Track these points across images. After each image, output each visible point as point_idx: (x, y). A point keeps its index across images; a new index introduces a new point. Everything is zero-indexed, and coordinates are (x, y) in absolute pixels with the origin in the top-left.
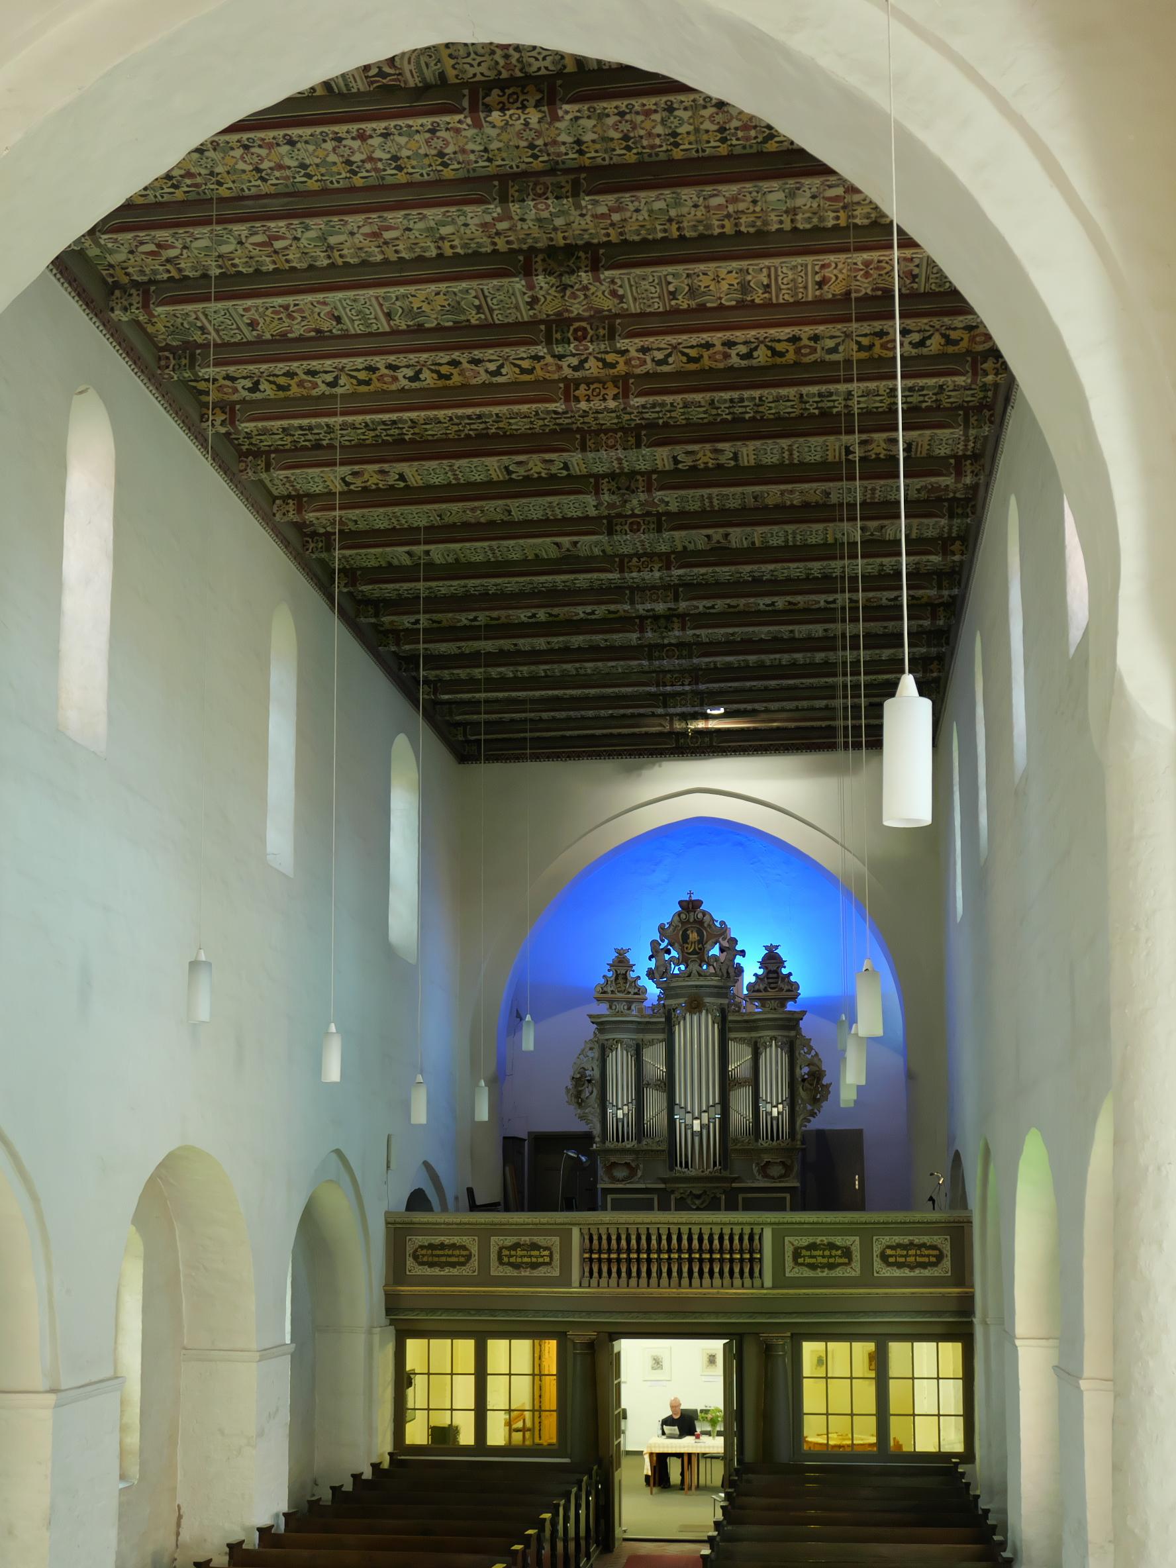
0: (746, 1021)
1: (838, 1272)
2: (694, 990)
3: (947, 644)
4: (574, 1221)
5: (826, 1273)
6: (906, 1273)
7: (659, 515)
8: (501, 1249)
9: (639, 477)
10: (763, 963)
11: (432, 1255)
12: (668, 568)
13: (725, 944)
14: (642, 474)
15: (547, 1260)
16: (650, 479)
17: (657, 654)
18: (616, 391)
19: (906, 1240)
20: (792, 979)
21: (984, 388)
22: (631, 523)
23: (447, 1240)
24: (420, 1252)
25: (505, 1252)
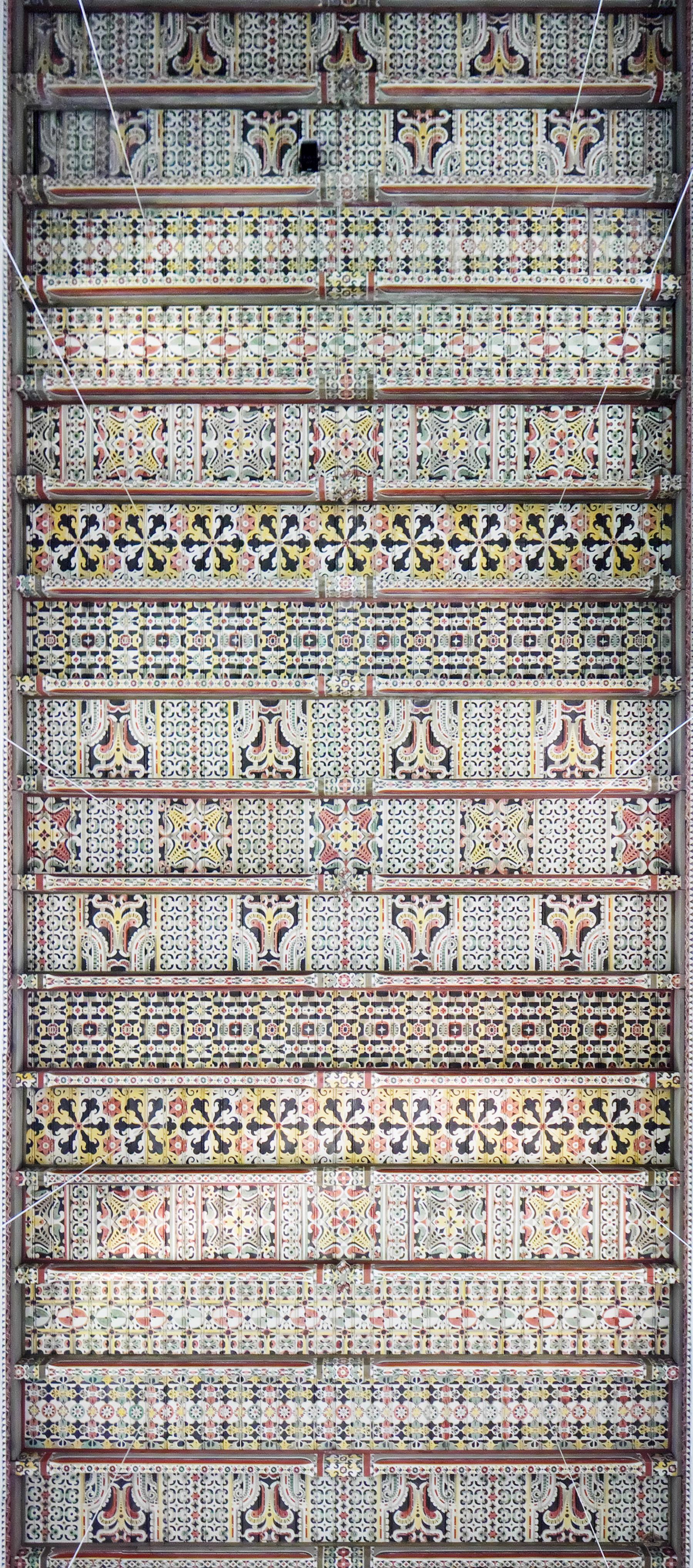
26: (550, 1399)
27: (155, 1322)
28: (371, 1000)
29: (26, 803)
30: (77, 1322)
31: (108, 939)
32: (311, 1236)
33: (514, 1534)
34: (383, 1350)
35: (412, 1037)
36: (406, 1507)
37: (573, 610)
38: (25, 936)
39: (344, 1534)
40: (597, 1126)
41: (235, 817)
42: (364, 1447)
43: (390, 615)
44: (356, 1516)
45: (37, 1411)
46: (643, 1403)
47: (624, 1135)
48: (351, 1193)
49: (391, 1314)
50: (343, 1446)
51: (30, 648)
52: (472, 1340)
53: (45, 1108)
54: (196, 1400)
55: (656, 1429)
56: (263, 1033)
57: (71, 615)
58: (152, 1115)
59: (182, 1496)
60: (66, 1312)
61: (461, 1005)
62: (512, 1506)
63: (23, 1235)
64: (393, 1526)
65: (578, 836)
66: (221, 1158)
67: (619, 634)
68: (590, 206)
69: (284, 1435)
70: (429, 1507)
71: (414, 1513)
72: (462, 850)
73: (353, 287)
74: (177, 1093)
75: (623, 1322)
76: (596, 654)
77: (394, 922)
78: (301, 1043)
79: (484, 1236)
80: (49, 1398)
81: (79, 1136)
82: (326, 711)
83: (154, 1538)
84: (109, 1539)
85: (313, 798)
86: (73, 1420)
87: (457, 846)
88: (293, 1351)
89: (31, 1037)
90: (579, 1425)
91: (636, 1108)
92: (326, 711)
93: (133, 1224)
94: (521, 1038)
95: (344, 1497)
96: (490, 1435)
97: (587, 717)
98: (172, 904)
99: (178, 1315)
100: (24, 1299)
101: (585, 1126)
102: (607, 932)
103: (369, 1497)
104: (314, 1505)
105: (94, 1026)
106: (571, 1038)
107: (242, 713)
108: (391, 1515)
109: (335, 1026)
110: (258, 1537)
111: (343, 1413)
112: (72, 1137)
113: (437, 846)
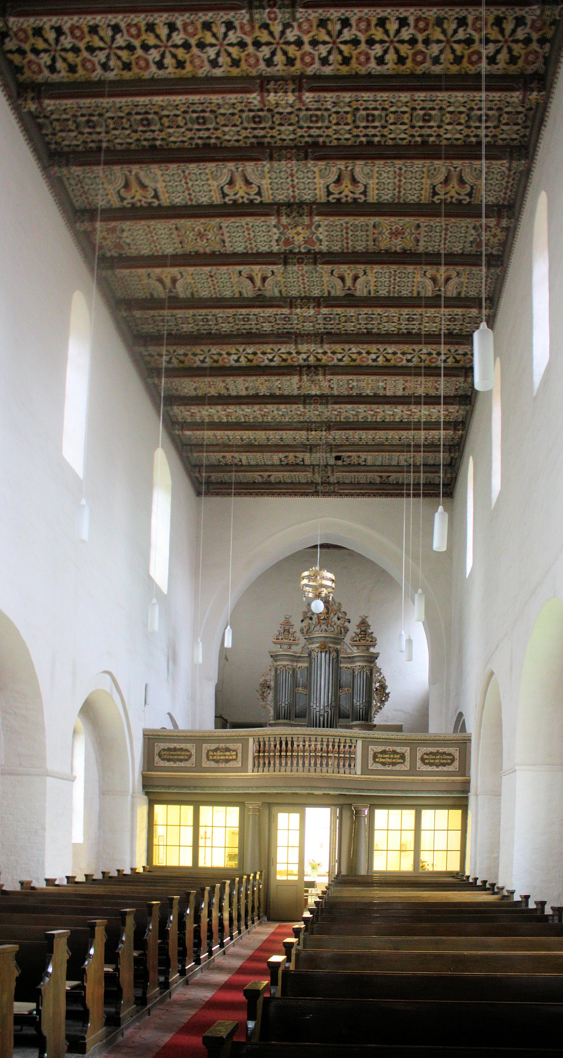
0: (349, 658)
1: (397, 768)
2: (323, 640)
3: (470, 404)
4: (251, 734)
5: (391, 768)
6: (434, 768)
7: (316, 254)
8: (208, 751)
9: (304, 206)
10: (359, 626)
11: (170, 755)
12: (319, 307)
13: (340, 615)
14: (307, 204)
15: (234, 757)
16: (311, 208)
17: (308, 401)
18: (293, 87)
19: (434, 750)
20: (374, 635)
21: (295, 658)
22: (298, 259)
23: (178, 746)
24: (162, 753)
25: (211, 753)
41: (371, 243)
57: (495, 136)
68: (217, 445)
73: (276, 92)
85: (320, 253)
89: (532, 113)
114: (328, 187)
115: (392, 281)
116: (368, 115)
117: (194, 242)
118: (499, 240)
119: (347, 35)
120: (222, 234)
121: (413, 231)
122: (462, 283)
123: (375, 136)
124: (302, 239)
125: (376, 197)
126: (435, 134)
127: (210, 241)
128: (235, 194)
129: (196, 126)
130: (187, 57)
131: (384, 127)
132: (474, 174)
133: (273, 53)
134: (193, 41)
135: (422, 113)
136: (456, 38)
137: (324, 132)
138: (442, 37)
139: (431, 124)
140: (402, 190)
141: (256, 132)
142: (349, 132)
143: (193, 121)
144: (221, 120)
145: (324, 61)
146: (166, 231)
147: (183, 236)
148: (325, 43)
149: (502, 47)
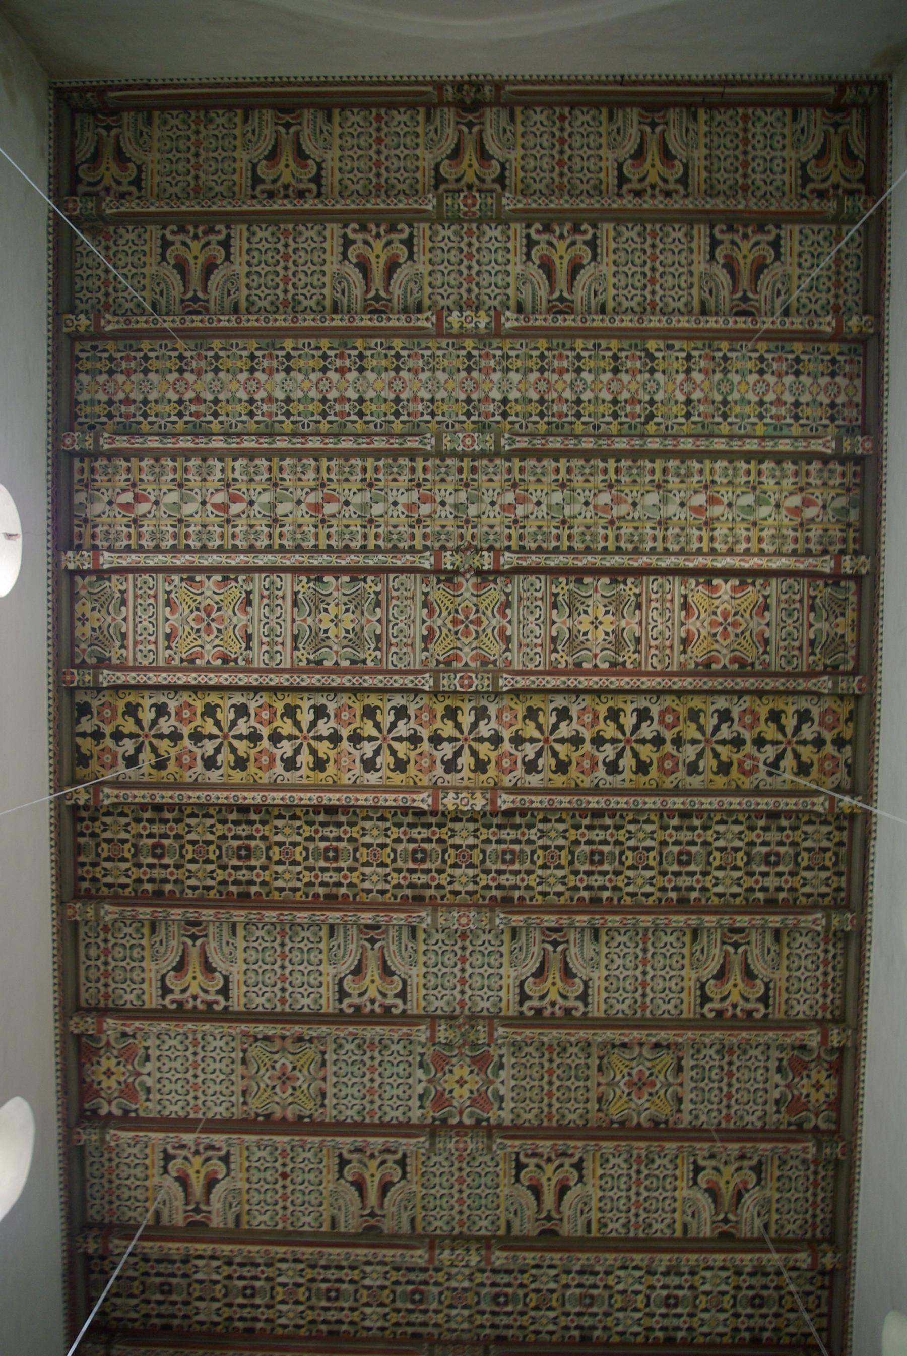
26: (216, 402)
27: (700, 500)
28: (432, 891)
29: (838, 1122)
30: (795, 501)
31: (747, 966)
32: (508, 604)
33: (260, 234)
34: (420, 463)
35: (383, 846)
36: (392, 267)
37: (202, 1323)
38: (845, 970)
39: (470, 233)
40: (161, 736)
41: (593, 1106)
42: (444, 343)
43: (409, 1324)
44: (453, 256)
45: (846, 389)
46: (104, 398)
47: (129, 726)
48: (458, 658)
49: (410, 507)
50: (469, 343)
51: (825, 1294)
52: (311, 475)
53: (828, 766)
54: (652, 402)
55: (89, 365)
56: (564, 853)
58: (700, 755)
59: (670, 281)
60: (810, 513)
61: (323, 884)
62: (263, 269)
63: (859, 609)
64: (409, 243)
65: (189, 1075)
66: (617, 702)
67: (147, 1295)
69: (542, 357)
70: (364, 267)
71: (383, 260)
72: (324, 1064)
74: (669, 782)
75: (128, 497)
76: (173, 1275)
77: (404, 982)
78: (517, 841)
79: (295, 603)
80: (833, 405)
81: (789, 730)
82: (484, 1223)
83: (704, 229)
84: (761, 229)
85: (499, 1126)
86: (803, 378)
87: (330, 1068)
88: (530, 463)
89: (843, 850)
90: (181, 371)
91: (115, 758)
92: (484, 1223)
93: (727, 622)
94: (253, 843)
95: (469, 279)
96: (288, 357)
97: (182, 1208)
98: (670, 1007)
99: (672, 509)
100: (860, 530)
101: (175, 737)
102: (153, 966)
103: (439, 280)
104: (507, 265)
105: (768, 863)
106: (193, 843)
107: (581, 1222)
108: (411, 256)
109: (476, 861)
110: (576, 229)
111: (469, 385)
112: (797, 729)
113: (355, 1069)
114: (522, 985)
115: (634, 1198)
116: (592, 853)
117: (269, 1091)
118: (827, 1096)
119: (564, 730)
120: (324, 1079)
121: (671, 1079)
122: (769, 1201)
123: (603, 888)
124: (467, 1095)
125: (603, 1007)
126: (698, 886)
127: (298, 1093)
128: (361, 995)
129: (322, 864)
130: (332, 754)
131: (617, 873)
132: (768, 958)
133: (457, 754)
134: (345, 733)
135: (676, 849)
136: (719, 736)
137: (523, 880)
138: (698, 736)
139: (692, 868)
140: (648, 991)
141: (414, 878)
142: (563, 880)
143: (317, 855)
144: (364, 855)
145: (531, 767)
146: (223, 1066)
147: (252, 1078)
148: (532, 740)
149: (784, 750)
